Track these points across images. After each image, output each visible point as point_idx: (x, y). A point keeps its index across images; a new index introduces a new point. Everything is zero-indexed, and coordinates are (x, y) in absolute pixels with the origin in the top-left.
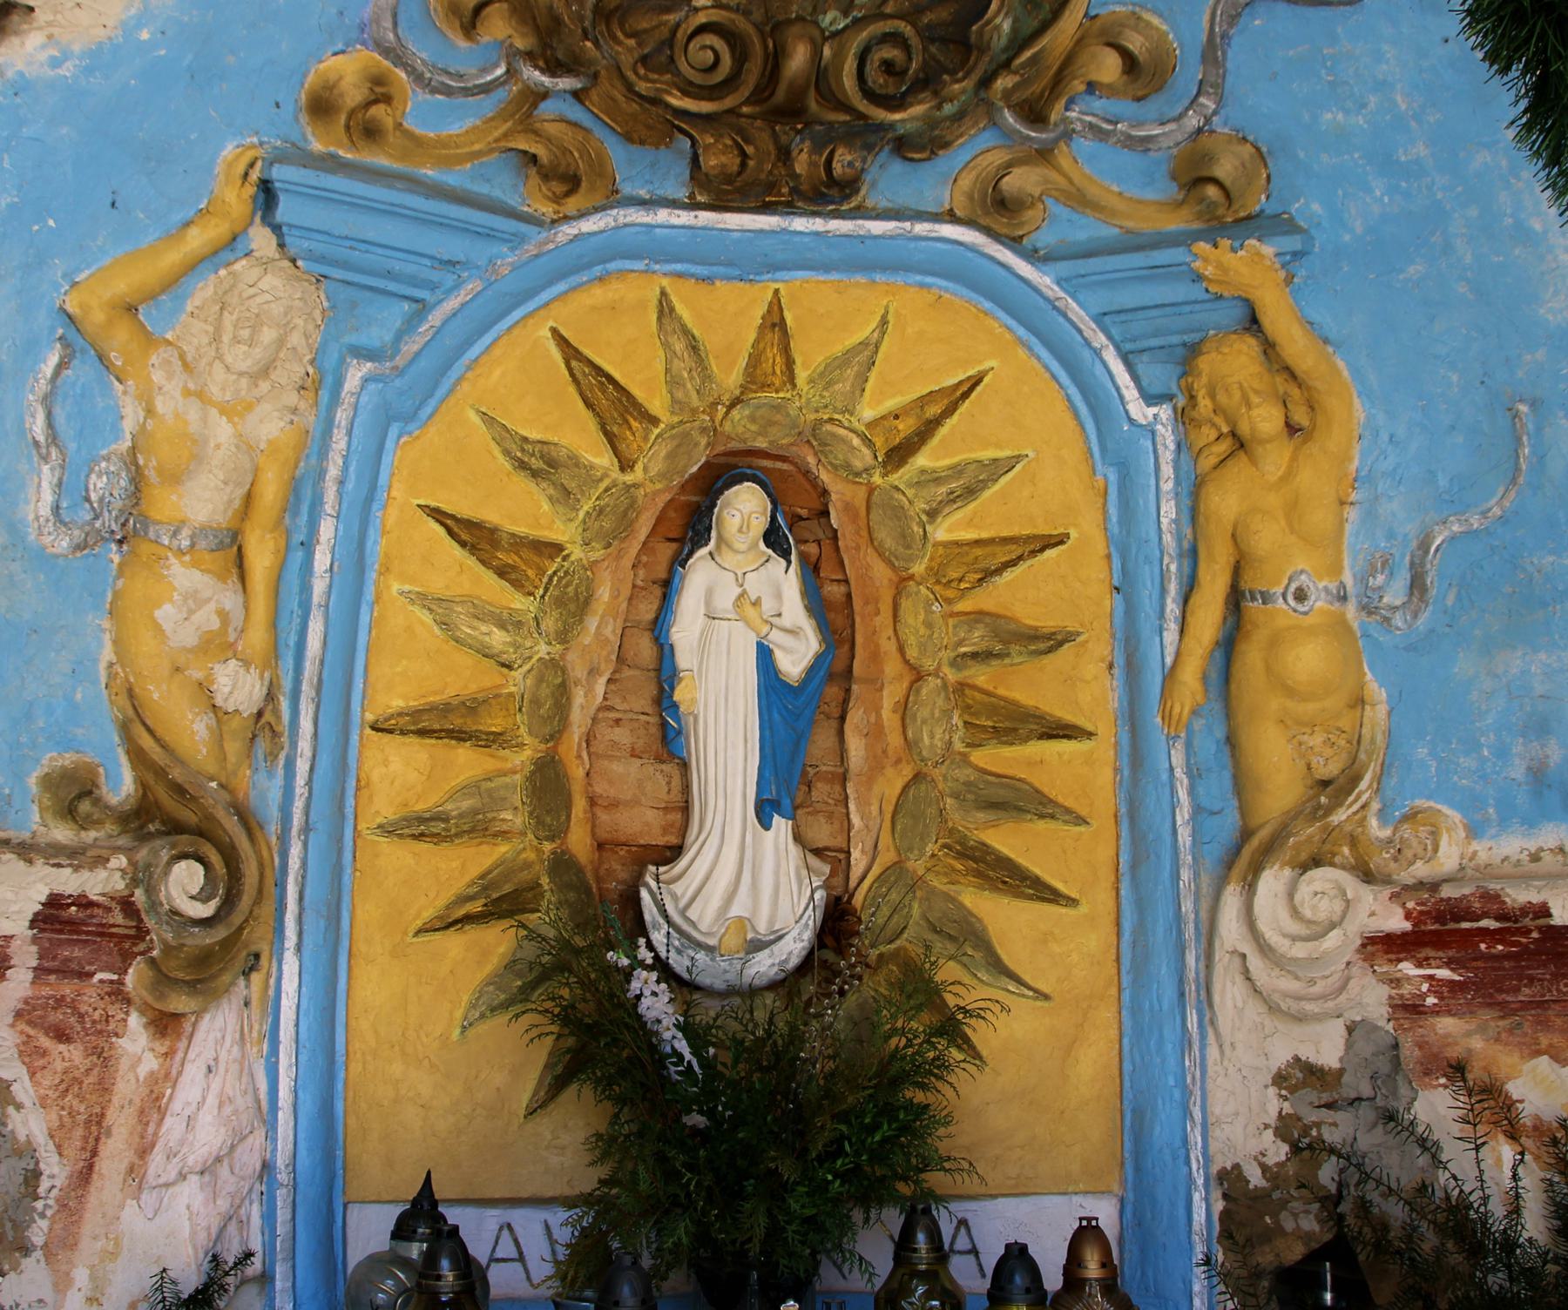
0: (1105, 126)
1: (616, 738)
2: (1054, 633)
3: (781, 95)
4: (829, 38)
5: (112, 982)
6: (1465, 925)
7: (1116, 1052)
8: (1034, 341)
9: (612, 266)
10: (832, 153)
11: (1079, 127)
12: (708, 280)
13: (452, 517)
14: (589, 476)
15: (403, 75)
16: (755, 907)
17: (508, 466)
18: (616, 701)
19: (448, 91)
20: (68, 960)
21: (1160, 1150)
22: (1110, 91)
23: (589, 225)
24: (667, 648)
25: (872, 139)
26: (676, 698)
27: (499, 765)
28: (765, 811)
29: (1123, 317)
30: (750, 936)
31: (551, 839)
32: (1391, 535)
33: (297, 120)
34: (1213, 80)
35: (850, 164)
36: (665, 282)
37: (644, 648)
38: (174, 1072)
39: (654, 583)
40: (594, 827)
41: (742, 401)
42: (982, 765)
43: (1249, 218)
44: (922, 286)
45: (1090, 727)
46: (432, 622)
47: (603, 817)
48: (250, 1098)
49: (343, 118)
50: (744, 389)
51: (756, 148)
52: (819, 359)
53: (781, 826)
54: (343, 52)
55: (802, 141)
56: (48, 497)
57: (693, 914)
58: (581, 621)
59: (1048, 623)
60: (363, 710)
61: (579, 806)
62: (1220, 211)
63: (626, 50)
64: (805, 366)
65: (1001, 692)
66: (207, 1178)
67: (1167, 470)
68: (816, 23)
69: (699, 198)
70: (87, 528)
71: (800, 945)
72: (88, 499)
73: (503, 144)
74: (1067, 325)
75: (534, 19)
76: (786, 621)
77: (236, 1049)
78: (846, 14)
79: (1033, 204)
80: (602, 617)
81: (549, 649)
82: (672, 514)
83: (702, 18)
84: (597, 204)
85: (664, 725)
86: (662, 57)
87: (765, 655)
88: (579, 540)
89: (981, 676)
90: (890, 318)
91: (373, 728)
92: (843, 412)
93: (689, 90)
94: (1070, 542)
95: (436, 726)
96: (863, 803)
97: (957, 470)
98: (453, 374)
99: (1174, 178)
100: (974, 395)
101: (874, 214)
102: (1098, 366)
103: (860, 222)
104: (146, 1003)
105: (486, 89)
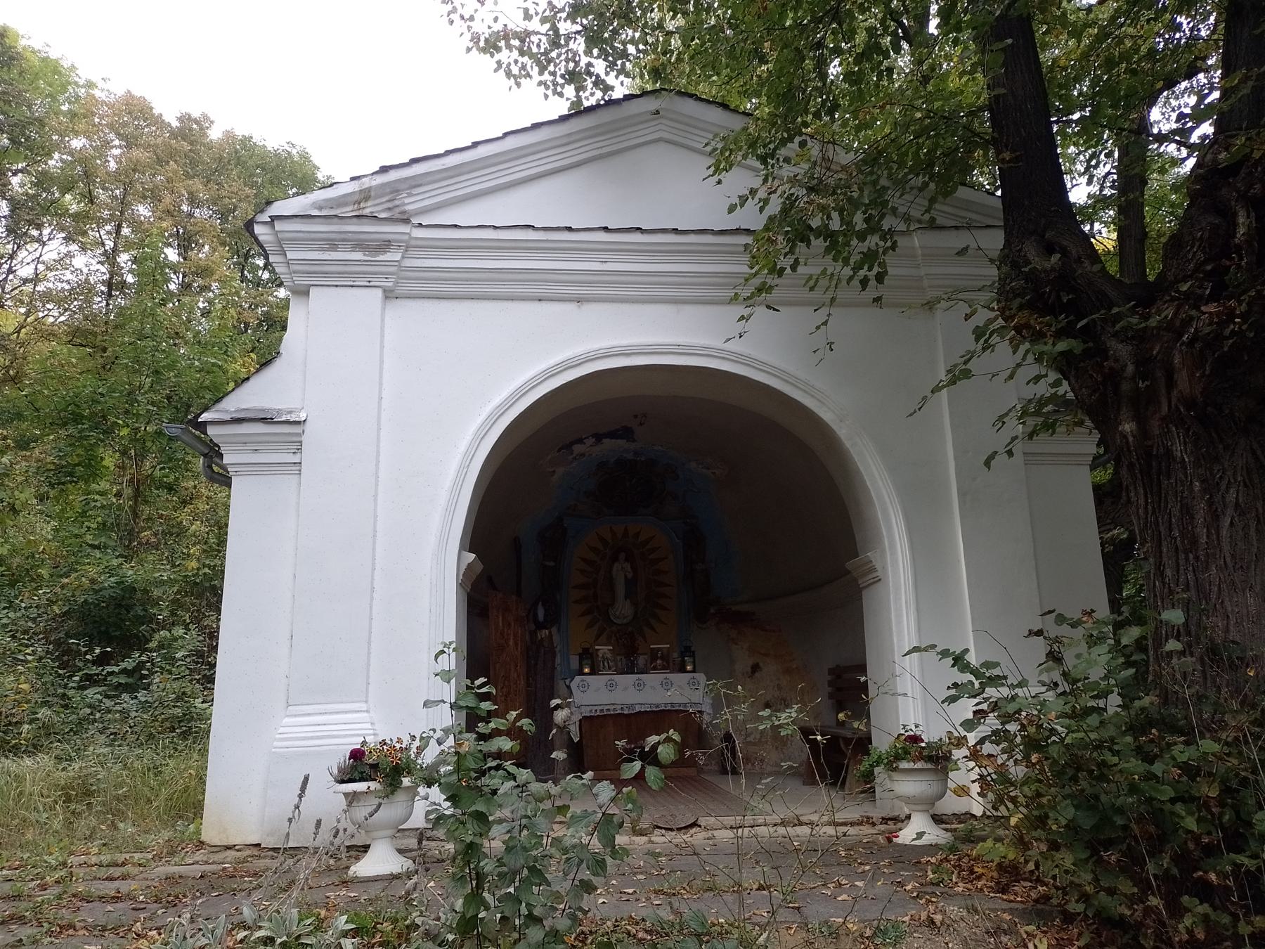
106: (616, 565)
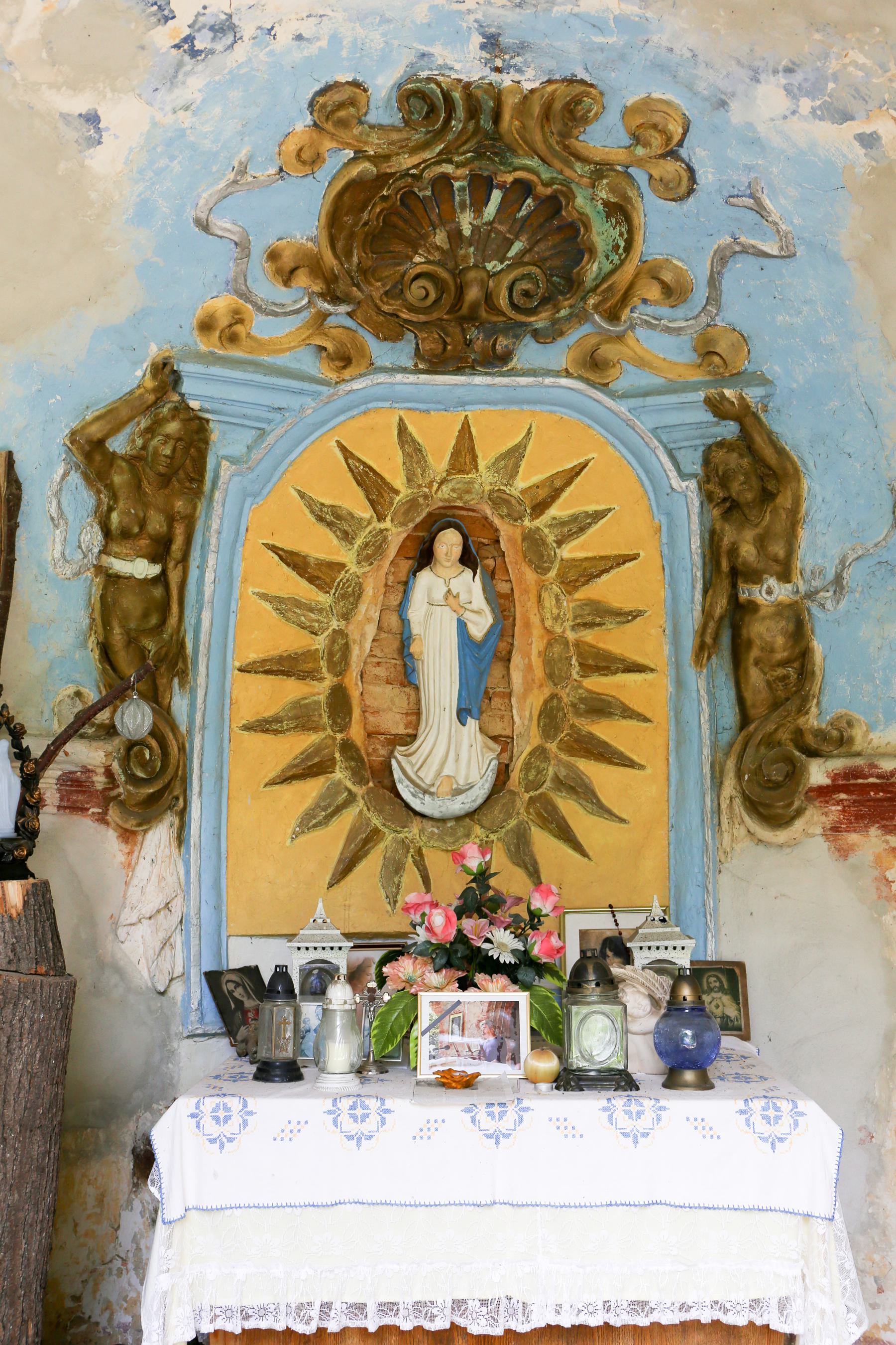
0: (654, 322)
1: (378, 673)
2: (631, 612)
3: (465, 310)
4: (492, 276)
5: (99, 813)
6: (860, 781)
7: (666, 854)
8: (617, 443)
9: (370, 406)
10: (496, 339)
11: (639, 322)
12: (427, 411)
13: (282, 549)
14: (360, 524)
15: (250, 307)
16: (457, 769)
17: (313, 519)
18: (377, 652)
19: (276, 314)
20: (76, 801)
21: (690, 910)
22: (656, 303)
23: (357, 385)
24: (406, 621)
25: (519, 331)
26: (412, 650)
27: (310, 690)
28: (462, 714)
29: (668, 430)
30: (454, 786)
31: (341, 731)
32: (824, 556)
33: (192, 334)
34: (714, 298)
35: (506, 346)
36: (402, 413)
37: (393, 620)
38: (133, 863)
39: (399, 583)
40: (365, 724)
41: (447, 480)
42: (590, 687)
43: (739, 373)
44: (551, 412)
45: (653, 666)
46: (272, 609)
47: (371, 719)
48: (175, 877)
49: (217, 333)
50: (449, 473)
51: (453, 340)
52: (493, 456)
53: (472, 724)
54: (217, 297)
55: (479, 333)
56: (59, 548)
57: (420, 774)
58: (356, 607)
59: (628, 606)
60: (233, 660)
61: (356, 713)
62: (721, 370)
63: (376, 289)
64: (484, 458)
65: (601, 645)
66: (152, 921)
67: (695, 519)
68: (484, 268)
69: (421, 366)
70: (80, 564)
71: (483, 792)
72: (80, 547)
73: (307, 342)
74: (635, 435)
75: (323, 274)
76: (475, 606)
77: (167, 850)
78: (502, 262)
79: (614, 365)
80: (369, 604)
81: (338, 623)
82: (409, 543)
83: (418, 270)
84: (362, 372)
85: (405, 665)
86: (396, 291)
87: (462, 626)
88: (355, 561)
89: (589, 636)
90: (533, 429)
91: (240, 670)
92: (506, 485)
93: (412, 309)
94: (640, 559)
95: (275, 668)
96: (521, 710)
97: (574, 518)
98: (282, 468)
99: (695, 350)
100: (583, 473)
101: (521, 372)
102: (654, 459)
103: (513, 378)
104: (117, 825)
105: (297, 312)
106: (425, 577)
